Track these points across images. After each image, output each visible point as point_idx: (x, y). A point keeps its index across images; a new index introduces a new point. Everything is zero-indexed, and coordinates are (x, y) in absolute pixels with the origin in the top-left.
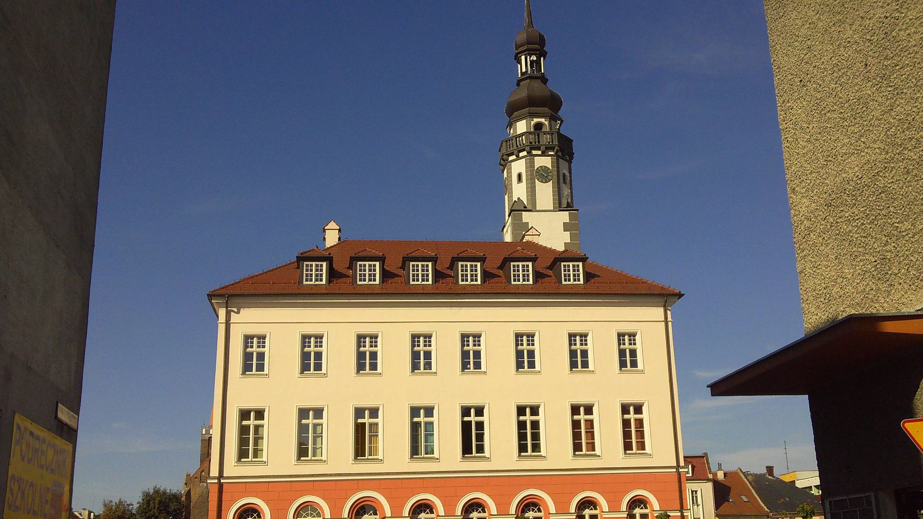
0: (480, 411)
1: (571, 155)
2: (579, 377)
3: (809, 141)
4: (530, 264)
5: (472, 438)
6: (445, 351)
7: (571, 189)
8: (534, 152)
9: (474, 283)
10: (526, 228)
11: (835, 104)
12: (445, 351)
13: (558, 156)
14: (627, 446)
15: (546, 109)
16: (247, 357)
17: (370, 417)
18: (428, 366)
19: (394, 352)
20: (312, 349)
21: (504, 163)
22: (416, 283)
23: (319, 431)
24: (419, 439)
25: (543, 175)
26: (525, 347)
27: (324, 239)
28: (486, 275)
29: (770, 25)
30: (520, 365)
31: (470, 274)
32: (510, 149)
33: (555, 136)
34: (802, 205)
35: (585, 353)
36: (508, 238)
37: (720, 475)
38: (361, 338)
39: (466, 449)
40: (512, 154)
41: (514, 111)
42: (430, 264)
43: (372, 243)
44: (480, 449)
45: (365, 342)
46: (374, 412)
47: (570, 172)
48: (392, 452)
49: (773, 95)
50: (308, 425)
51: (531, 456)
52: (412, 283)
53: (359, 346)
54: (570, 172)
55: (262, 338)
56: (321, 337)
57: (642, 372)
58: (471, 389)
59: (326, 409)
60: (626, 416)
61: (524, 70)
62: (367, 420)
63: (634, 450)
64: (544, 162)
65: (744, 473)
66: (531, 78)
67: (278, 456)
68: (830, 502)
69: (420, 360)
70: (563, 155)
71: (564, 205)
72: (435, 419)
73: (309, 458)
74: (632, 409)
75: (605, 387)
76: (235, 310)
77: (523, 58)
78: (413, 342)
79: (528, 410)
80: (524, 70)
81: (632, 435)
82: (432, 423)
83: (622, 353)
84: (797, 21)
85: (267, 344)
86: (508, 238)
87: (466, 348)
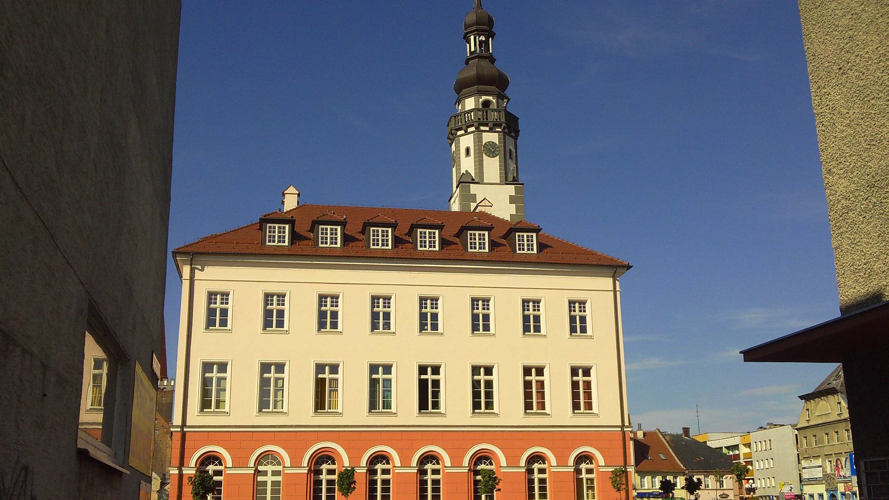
0: (436, 370)
1: (517, 132)
2: (532, 341)
3: (848, 126)
4: (486, 233)
5: (428, 395)
6: (405, 313)
7: (516, 164)
8: (482, 128)
9: (432, 249)
10: (473, 198)
11: (881, 92)
12: (405, 313)
13: (504, 133)
14: (576, 406)
15: (493, 88)
16: (211, 313)
17: (219, 372)
18: (387, 326)
19: (301, 311)
20: (218, 305)
21: (452, 137)
22: (423, 249)
23: (280, 384)
24: (378, 395)
25: (490, 150)
26: (480, 311)
27: (283, 203)
28: (444, 243)
29: (804, 15)
30: (475, 328)
31: (429, 240)
32: (455, 126)
33: (503, 114)
34: (838, 185)
35: (537, 319)
36: (455, 207)
37: (640, 435)
38: (322, 298)
39: (423, 405)
40: (460, 129)
41: (462, 88)
42: (339, 228)
43: (383, 210)
44: (436, 405)
45: (326, 302)
46: (334, 369)
47: (516, 149)
48: (351, 406)
49: (807, 82)
50: (269, 379)
51: (484, 413)
52: (372, 247)
53: (320, 305)
54: (516, 149)
55: (225, 295)
56: (284, 296)
57: (591, 337)
58: (428, 348)
59: (287, 364)
60: (575, 378)
61: (473, 49)
62: (327, 375)
63: (582, 410)
64: (491, 137)
65: (661, 433)
66: (479, 57)
67: (240, 406)
68: (865, 463)
69: (380, 320)
70: (510, 132)
71: (510, 178)
72: (339, 376)
73: (271, 410)
74: (580, 371)
75: (556, 351)
76: (200, 267)
77: (472, 38)
78: (373, 303)
79: (533, 371)
80: (473, 49)
81: (581, 396)
82: (390, 380)
83: (572, 319)
84: (837, 12)
85: (230, 301)
86: (455, 207)
87: (376, 309)
